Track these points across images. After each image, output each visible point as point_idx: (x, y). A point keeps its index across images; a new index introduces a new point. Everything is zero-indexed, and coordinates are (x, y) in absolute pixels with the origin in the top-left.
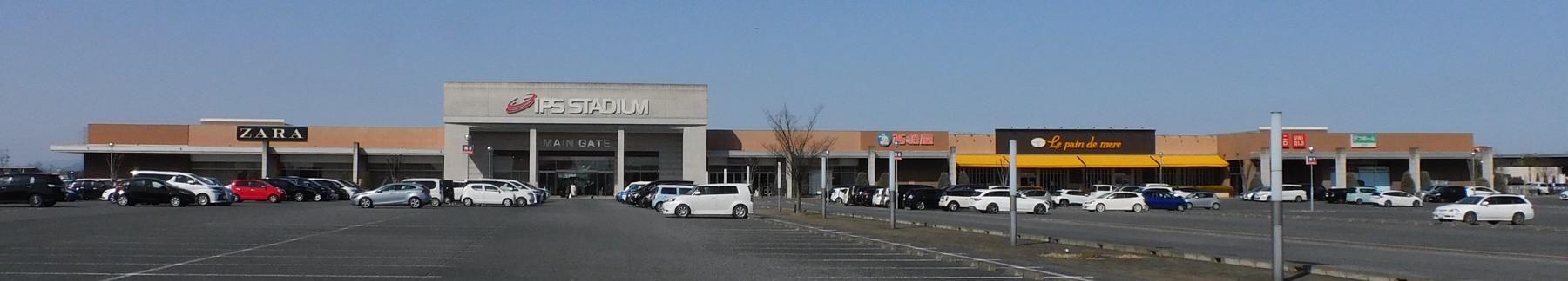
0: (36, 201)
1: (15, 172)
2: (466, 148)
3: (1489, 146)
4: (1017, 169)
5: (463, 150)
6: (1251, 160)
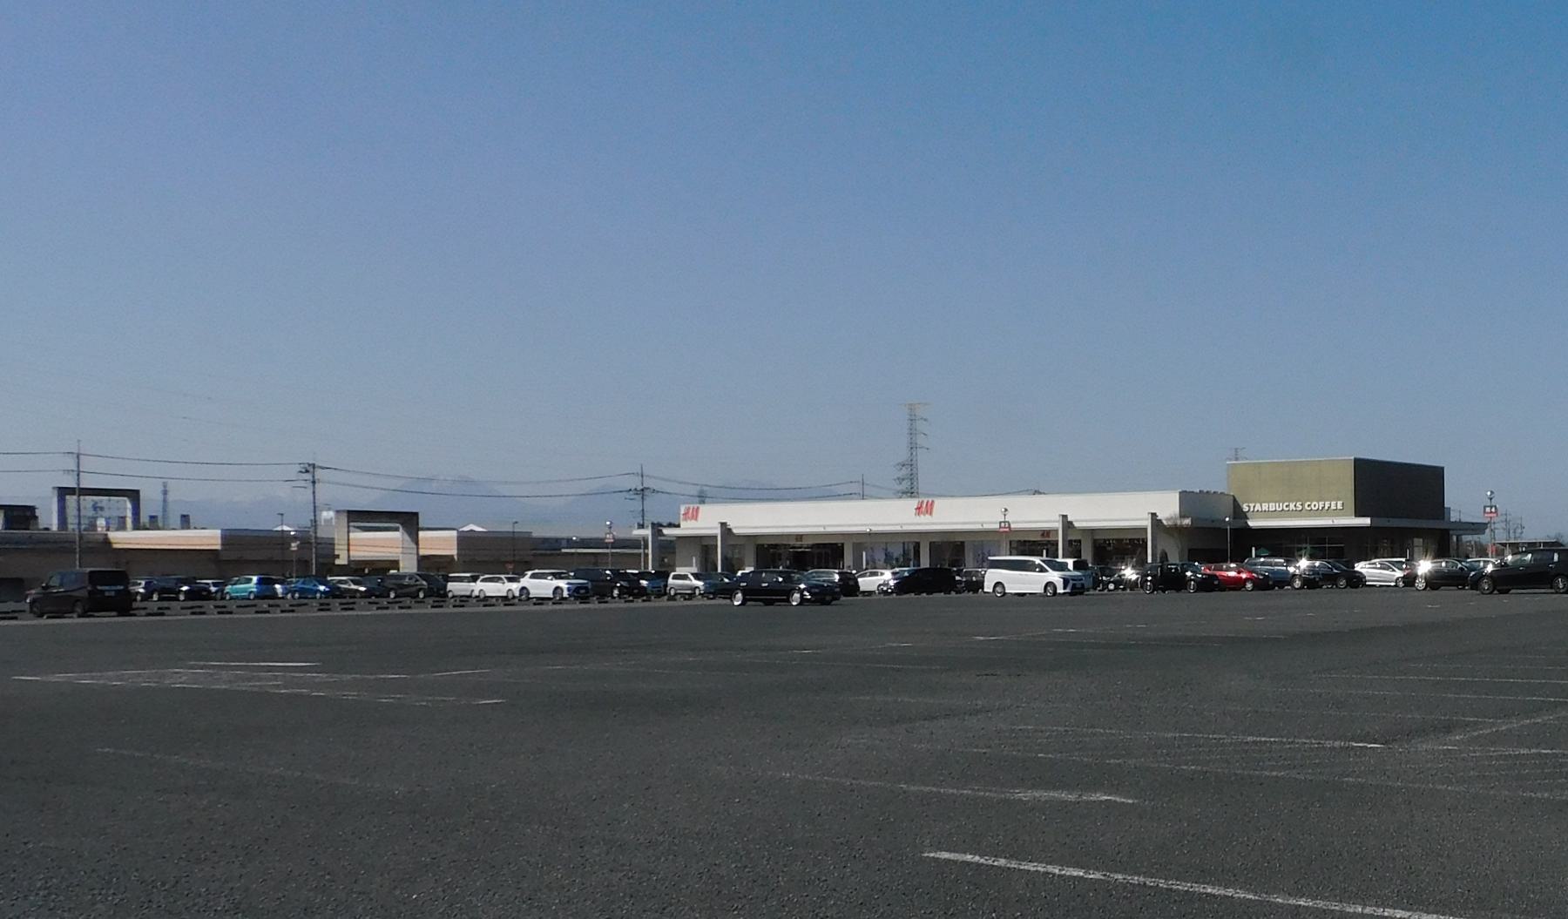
0: (1561, 586)
1: (1531, 547)
2: (1488, 509)
3: (163, 488)
4: (1190, 550)
5: (1485, 512)
6: (723, 525)
